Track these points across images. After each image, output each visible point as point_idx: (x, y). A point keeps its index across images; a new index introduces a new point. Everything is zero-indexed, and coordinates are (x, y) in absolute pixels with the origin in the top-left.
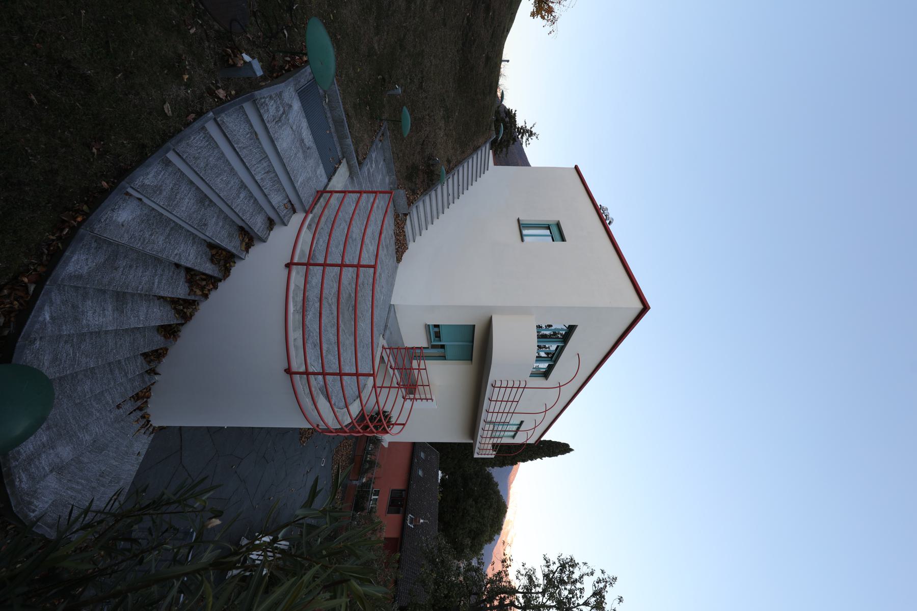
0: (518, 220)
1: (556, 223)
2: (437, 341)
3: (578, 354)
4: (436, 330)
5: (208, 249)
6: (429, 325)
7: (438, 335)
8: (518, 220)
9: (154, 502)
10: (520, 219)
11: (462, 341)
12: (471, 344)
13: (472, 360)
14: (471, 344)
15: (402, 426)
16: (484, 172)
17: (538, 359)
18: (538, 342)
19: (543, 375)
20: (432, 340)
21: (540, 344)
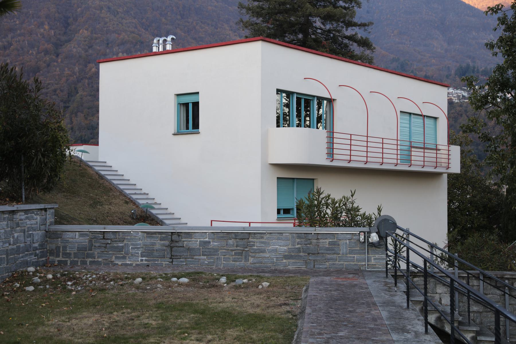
0: (174, 134)
1: (176, 96)
2: (293, 212)
3: (305, 79)
4: (282, 212)
5: (368, 37)
6: (278, 218)
7: (287, 211)
8: (174, 134)
9: (69, 93)
10: (173, 133)
11: (293, 189)
12: (295, 180)
13: (313, 179)
14: (295, 180)
15: (410, 251)
16: (170, 214)
17: (279, 219)
18: (293, 126)
19: (331, 103)
20: (293, 216)
21: (295, 125)
